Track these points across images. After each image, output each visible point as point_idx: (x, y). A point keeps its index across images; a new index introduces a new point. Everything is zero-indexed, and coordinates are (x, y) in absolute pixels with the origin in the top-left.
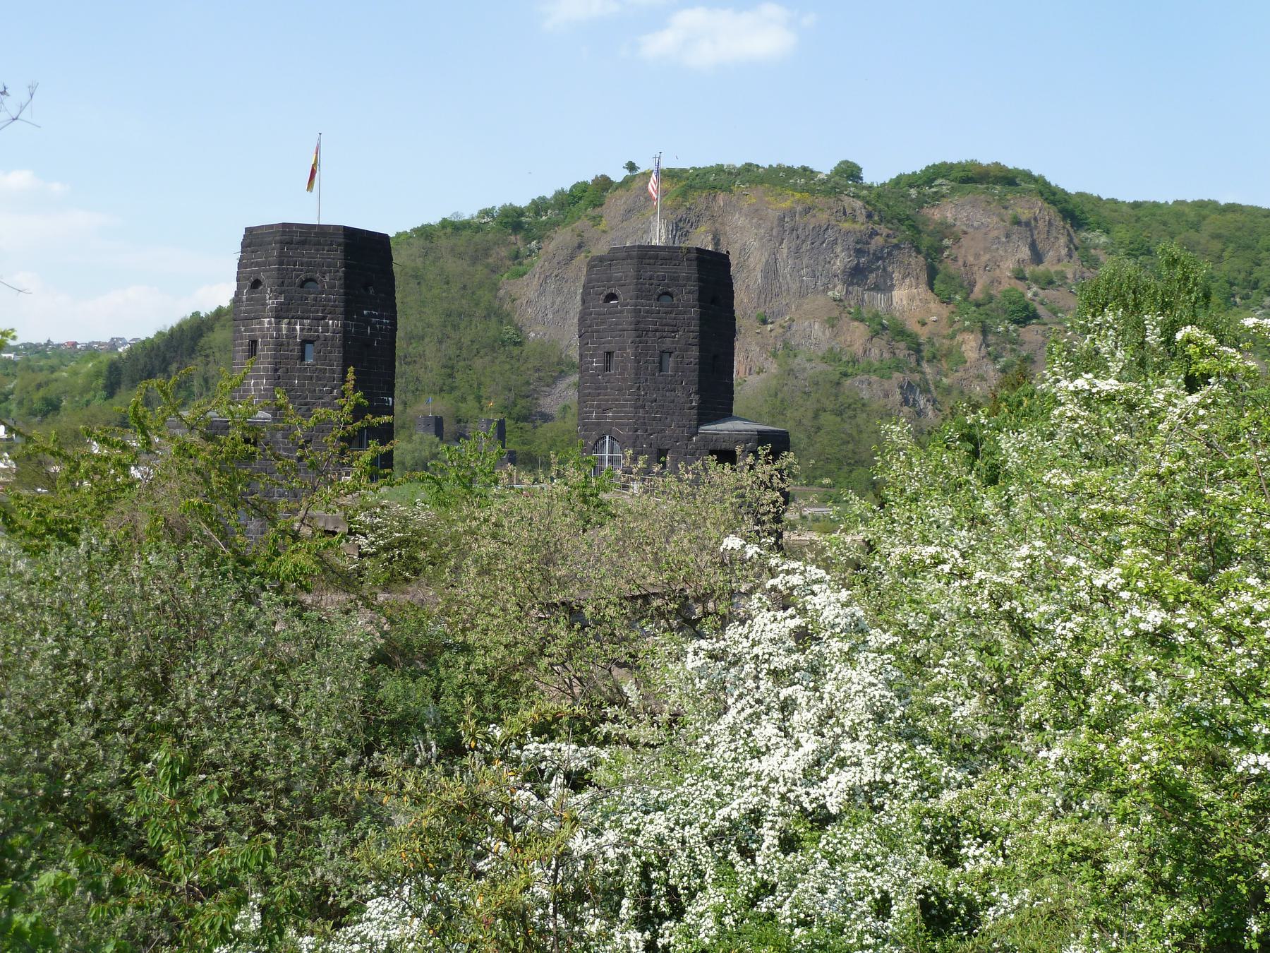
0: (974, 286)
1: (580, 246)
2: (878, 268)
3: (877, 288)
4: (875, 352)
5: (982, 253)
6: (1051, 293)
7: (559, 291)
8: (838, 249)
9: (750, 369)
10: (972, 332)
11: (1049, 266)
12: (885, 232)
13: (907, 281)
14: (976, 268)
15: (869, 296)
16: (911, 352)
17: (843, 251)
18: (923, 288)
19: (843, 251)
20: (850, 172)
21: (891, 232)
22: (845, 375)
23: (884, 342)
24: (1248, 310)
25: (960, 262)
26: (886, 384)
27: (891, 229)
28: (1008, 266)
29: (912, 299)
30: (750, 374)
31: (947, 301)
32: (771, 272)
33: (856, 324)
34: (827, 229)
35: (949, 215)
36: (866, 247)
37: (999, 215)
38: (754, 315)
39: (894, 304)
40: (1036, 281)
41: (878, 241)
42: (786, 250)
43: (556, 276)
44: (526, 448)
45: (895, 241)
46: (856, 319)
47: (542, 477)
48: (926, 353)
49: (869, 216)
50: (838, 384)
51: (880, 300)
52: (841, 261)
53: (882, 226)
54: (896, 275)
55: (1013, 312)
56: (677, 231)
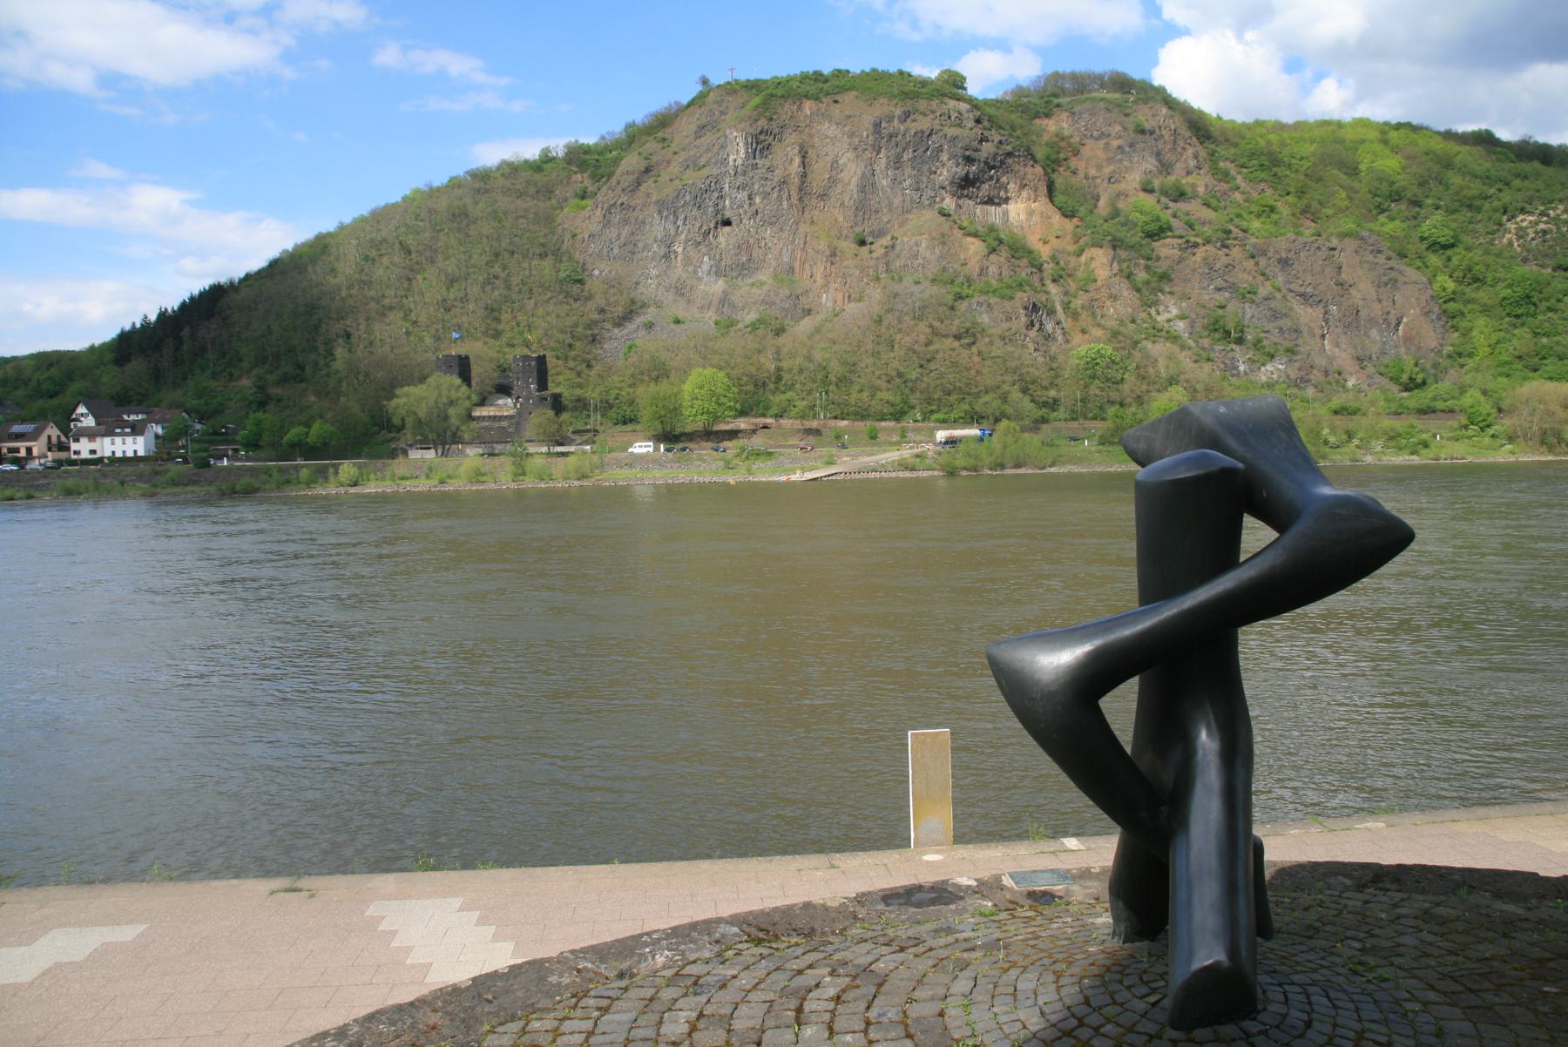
0: (1098, 200)
1: (648, 170)
2: (991, 178)
3: (990, 201)
4: (993, 270)
5: (1104, 164)
6: (1182, 206)
7: (626, 222)
8: (944, 157)
9: (849, 297)
10: (1101, 247)
11: (1177, 177)
12: (997, 138)
13: (1024, 194)
14: (1099, 181)
15: (982, 211)
16: (1034, 270)
17: (949, 159)
18: (1043, 199)
19: (949, 159)
20: (953, 84)
21: (1003, 138)
22: (959, 297)
23: (1002, 259)
24: (926, 853)
25: (1081, 175)
26: (1008, 305)
27: (1003, 135)
28: (1134, 179)
29: (1030, 213)
30: (849, 301)
31: (1068, 214)
32: (867, 185)
33: (969, 239)
34: (930, 135)
35: (1065, 125)
36: (975, 155)
37: (1121, 124)
38: (852, 236)
39: (1011, 219)
40: (1165, 193)
41: (987, 149)
42: (884, 161)
43: (622, 204)
44: (578, 392)
45: (1009, 148)
46: (970, 235)
47: (340, 326)
48: (1049, 268)
49: (978, 121)
50: (952, 308)
51: (994, 214)
52: (948, 171)
53: (993, 132)
54: (1011, 186)
55: (1147, 224)
56: (757, 143)
